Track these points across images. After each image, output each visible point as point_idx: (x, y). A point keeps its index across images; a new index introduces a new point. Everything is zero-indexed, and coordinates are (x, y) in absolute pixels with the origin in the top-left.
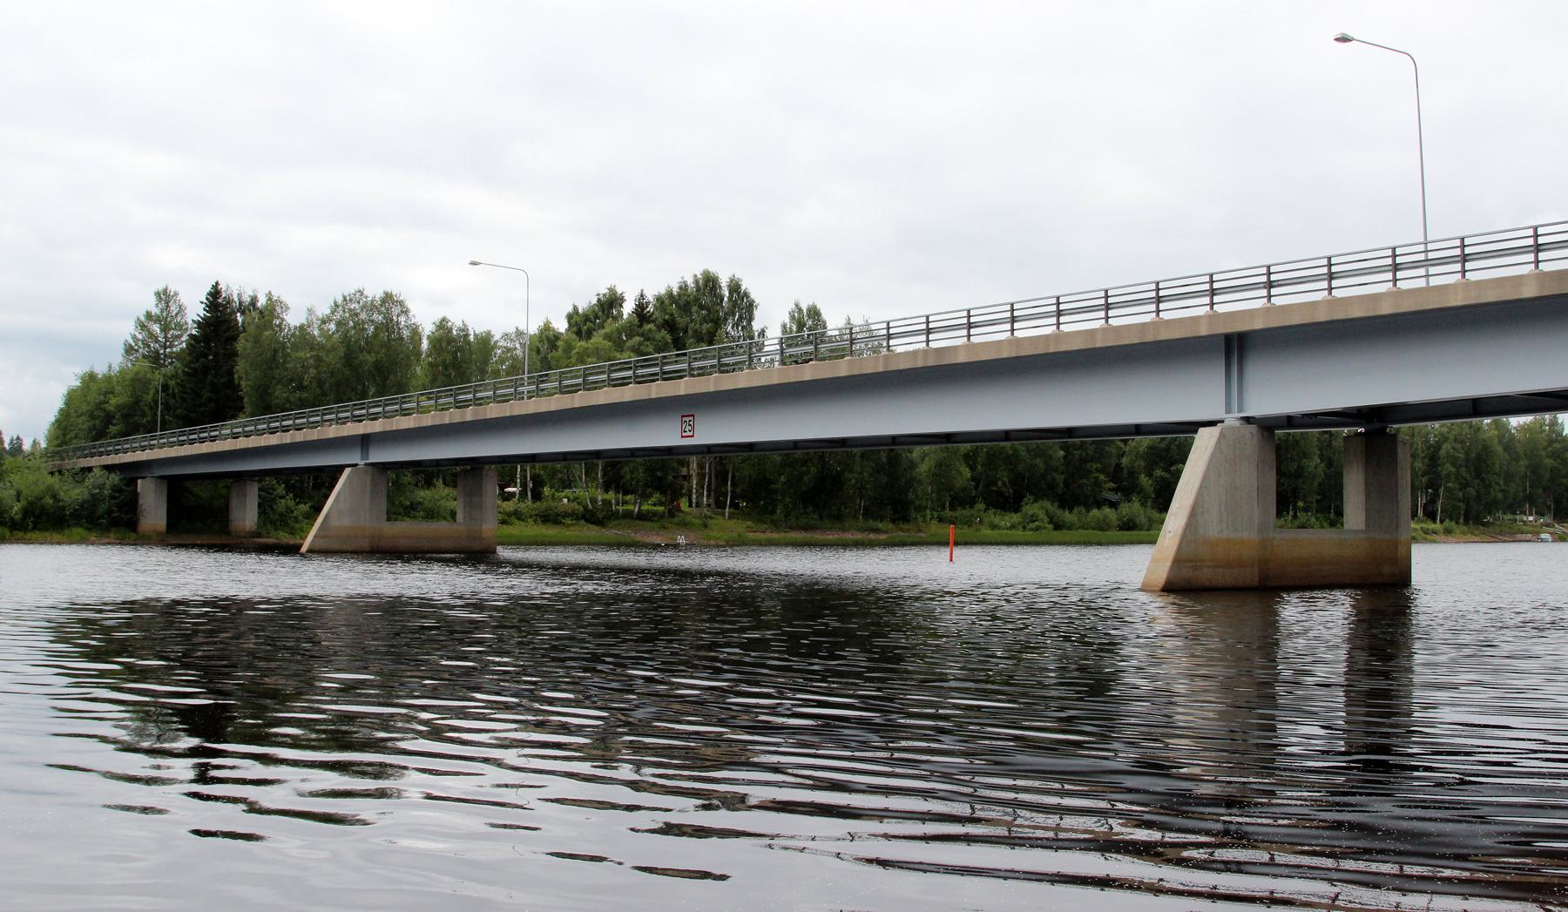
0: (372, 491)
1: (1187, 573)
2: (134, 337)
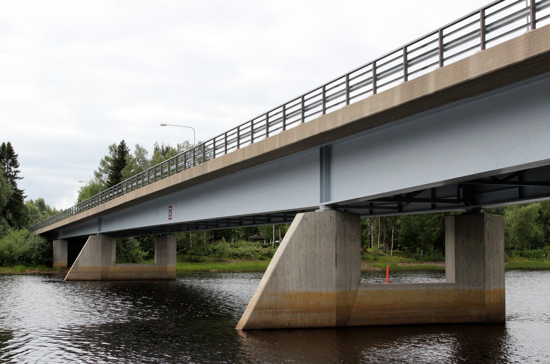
0: (102, 248)
1: (267, 318)
2: (100, 169)
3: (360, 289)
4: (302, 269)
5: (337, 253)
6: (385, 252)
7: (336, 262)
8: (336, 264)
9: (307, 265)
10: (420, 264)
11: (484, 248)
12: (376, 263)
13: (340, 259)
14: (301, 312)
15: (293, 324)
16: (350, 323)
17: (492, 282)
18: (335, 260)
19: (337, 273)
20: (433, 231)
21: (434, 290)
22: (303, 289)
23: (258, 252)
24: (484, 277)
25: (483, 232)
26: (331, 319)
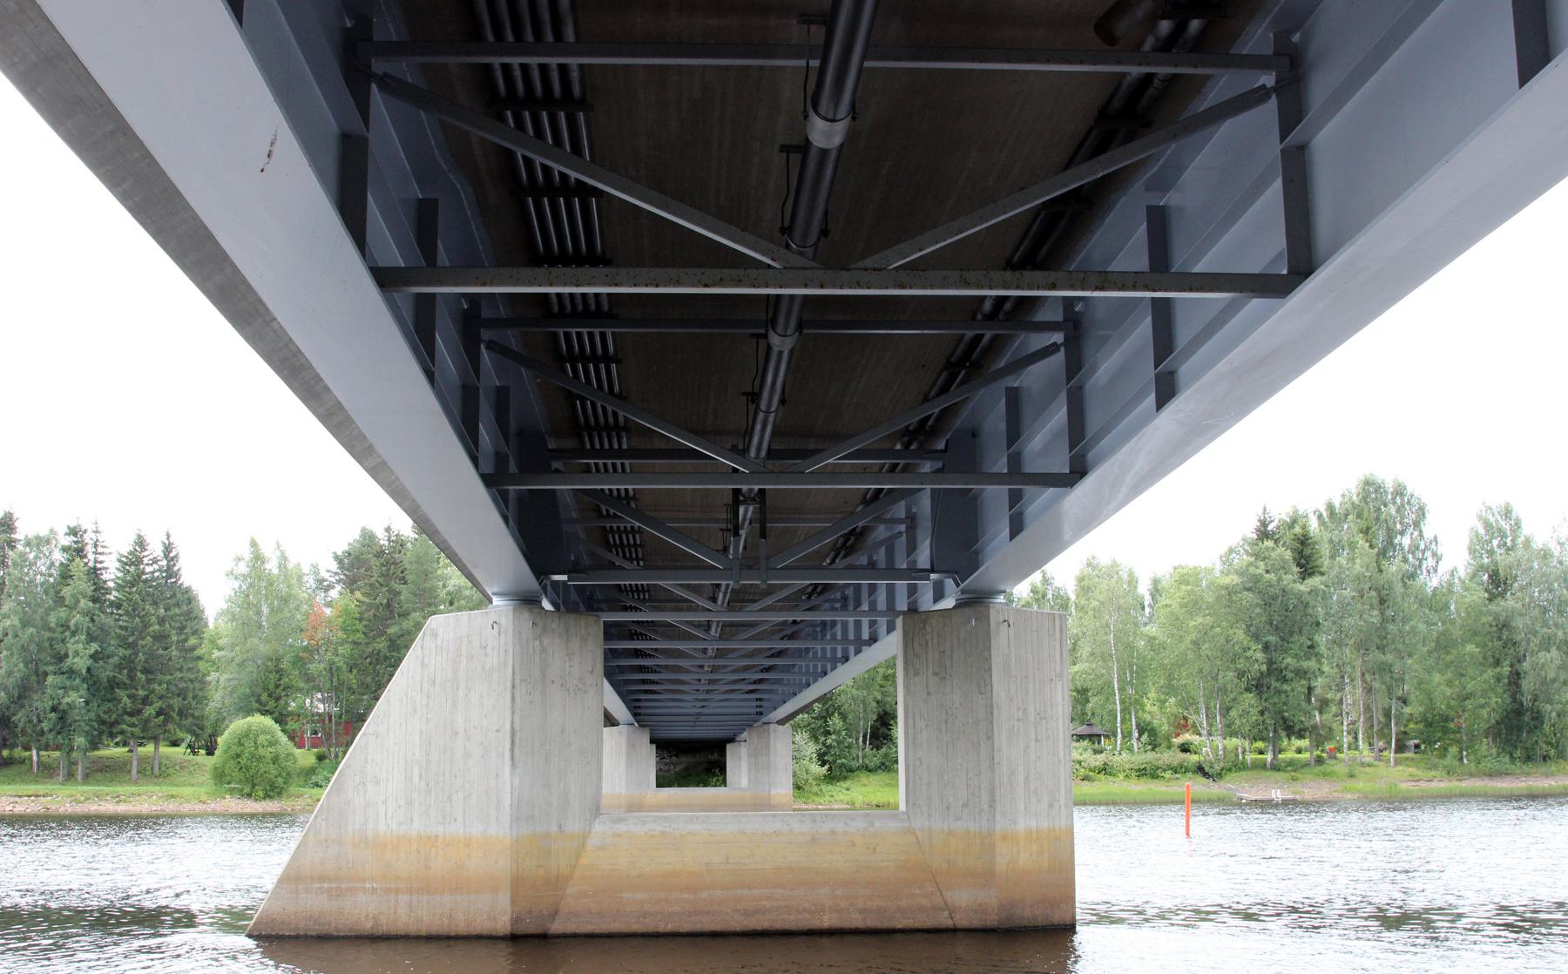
3: (600, 828)
4: (416, 772)
5: (517, 727)
6: (1379, 759)
7: (512, 750)
8: (512, 759)
9: (429, 761)
10: (1455, 784)
11: (990, 708)
12: (1352, 784)
13: (521, 744)
14: (410, 891)
15: (385, 927)
16: (556, 927)
17: (1021, 807)
18: (508, 746)
19: (517, 781)
20: (1482, 707)
21: (833, 832)
22: (417, 827)
23: (1080, 762)
24: (992, 793)
25: (988, 659)
26: (497, 914)
